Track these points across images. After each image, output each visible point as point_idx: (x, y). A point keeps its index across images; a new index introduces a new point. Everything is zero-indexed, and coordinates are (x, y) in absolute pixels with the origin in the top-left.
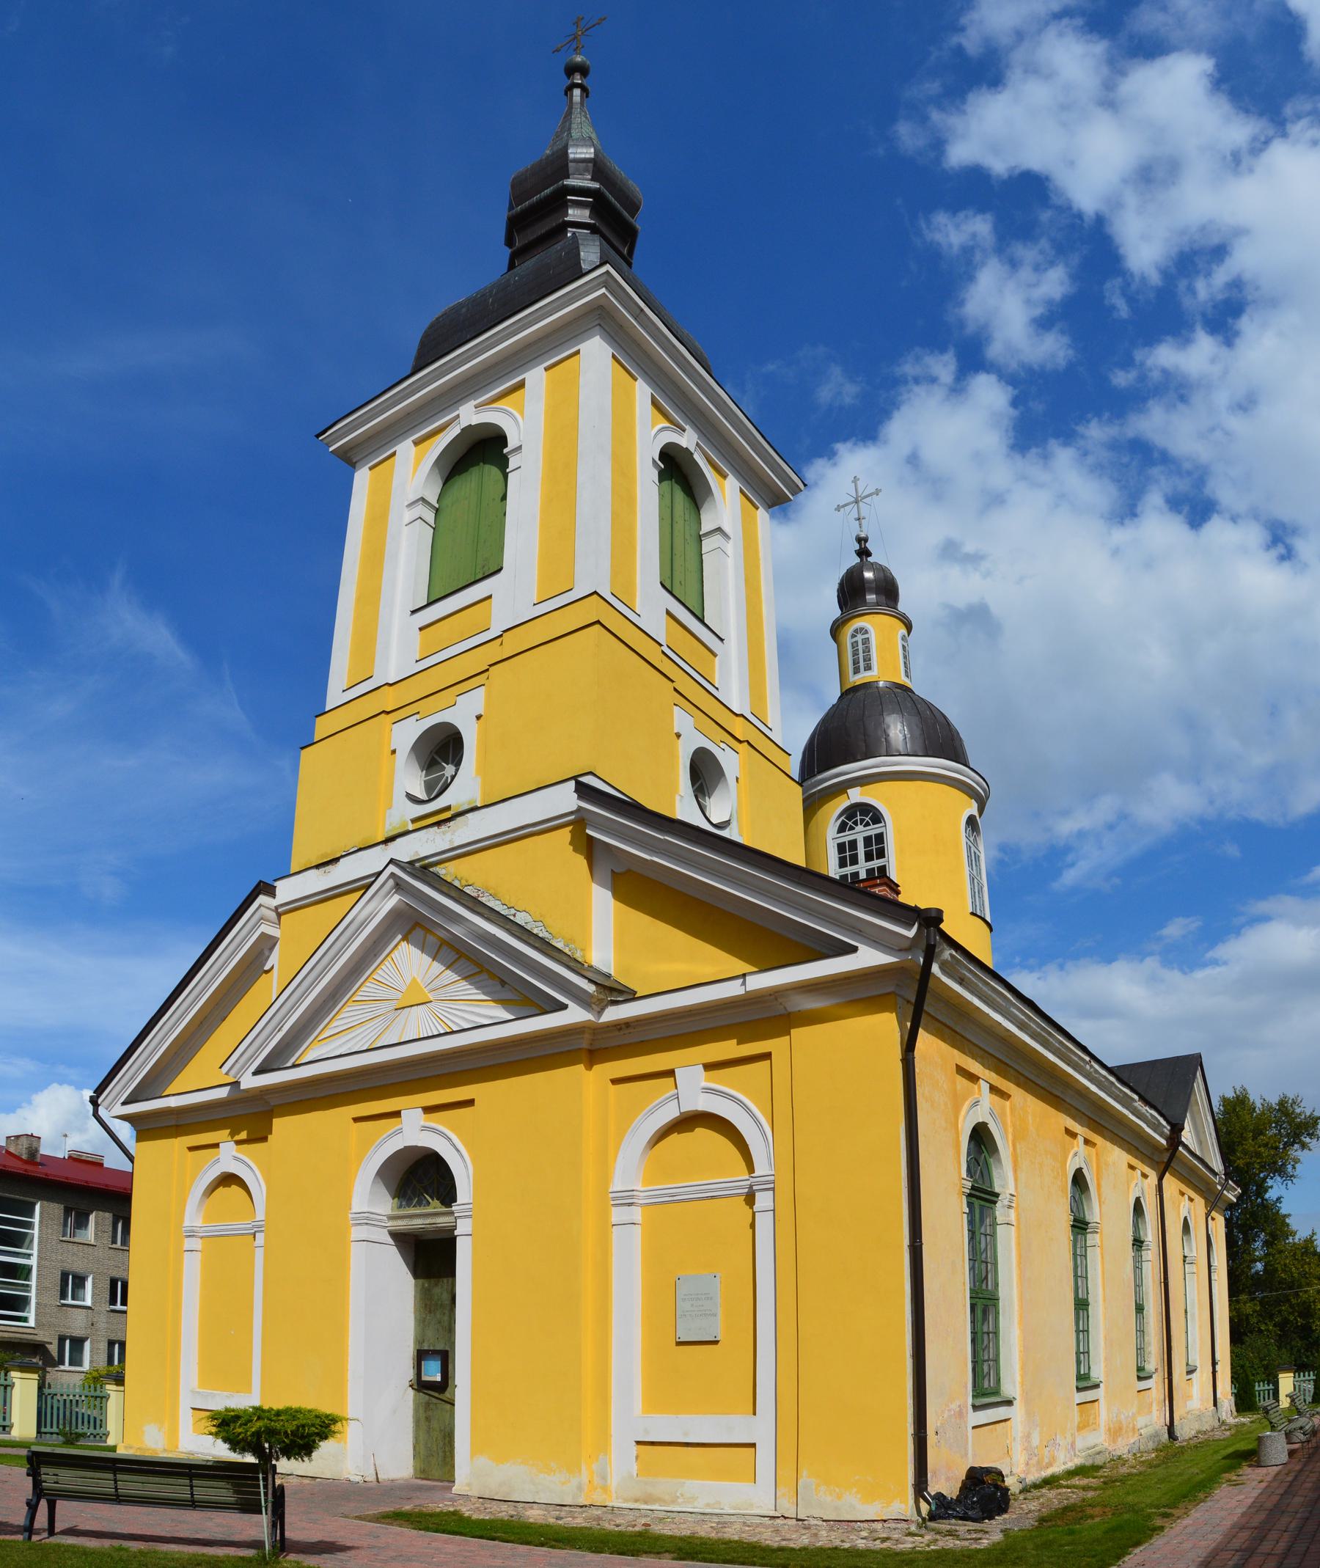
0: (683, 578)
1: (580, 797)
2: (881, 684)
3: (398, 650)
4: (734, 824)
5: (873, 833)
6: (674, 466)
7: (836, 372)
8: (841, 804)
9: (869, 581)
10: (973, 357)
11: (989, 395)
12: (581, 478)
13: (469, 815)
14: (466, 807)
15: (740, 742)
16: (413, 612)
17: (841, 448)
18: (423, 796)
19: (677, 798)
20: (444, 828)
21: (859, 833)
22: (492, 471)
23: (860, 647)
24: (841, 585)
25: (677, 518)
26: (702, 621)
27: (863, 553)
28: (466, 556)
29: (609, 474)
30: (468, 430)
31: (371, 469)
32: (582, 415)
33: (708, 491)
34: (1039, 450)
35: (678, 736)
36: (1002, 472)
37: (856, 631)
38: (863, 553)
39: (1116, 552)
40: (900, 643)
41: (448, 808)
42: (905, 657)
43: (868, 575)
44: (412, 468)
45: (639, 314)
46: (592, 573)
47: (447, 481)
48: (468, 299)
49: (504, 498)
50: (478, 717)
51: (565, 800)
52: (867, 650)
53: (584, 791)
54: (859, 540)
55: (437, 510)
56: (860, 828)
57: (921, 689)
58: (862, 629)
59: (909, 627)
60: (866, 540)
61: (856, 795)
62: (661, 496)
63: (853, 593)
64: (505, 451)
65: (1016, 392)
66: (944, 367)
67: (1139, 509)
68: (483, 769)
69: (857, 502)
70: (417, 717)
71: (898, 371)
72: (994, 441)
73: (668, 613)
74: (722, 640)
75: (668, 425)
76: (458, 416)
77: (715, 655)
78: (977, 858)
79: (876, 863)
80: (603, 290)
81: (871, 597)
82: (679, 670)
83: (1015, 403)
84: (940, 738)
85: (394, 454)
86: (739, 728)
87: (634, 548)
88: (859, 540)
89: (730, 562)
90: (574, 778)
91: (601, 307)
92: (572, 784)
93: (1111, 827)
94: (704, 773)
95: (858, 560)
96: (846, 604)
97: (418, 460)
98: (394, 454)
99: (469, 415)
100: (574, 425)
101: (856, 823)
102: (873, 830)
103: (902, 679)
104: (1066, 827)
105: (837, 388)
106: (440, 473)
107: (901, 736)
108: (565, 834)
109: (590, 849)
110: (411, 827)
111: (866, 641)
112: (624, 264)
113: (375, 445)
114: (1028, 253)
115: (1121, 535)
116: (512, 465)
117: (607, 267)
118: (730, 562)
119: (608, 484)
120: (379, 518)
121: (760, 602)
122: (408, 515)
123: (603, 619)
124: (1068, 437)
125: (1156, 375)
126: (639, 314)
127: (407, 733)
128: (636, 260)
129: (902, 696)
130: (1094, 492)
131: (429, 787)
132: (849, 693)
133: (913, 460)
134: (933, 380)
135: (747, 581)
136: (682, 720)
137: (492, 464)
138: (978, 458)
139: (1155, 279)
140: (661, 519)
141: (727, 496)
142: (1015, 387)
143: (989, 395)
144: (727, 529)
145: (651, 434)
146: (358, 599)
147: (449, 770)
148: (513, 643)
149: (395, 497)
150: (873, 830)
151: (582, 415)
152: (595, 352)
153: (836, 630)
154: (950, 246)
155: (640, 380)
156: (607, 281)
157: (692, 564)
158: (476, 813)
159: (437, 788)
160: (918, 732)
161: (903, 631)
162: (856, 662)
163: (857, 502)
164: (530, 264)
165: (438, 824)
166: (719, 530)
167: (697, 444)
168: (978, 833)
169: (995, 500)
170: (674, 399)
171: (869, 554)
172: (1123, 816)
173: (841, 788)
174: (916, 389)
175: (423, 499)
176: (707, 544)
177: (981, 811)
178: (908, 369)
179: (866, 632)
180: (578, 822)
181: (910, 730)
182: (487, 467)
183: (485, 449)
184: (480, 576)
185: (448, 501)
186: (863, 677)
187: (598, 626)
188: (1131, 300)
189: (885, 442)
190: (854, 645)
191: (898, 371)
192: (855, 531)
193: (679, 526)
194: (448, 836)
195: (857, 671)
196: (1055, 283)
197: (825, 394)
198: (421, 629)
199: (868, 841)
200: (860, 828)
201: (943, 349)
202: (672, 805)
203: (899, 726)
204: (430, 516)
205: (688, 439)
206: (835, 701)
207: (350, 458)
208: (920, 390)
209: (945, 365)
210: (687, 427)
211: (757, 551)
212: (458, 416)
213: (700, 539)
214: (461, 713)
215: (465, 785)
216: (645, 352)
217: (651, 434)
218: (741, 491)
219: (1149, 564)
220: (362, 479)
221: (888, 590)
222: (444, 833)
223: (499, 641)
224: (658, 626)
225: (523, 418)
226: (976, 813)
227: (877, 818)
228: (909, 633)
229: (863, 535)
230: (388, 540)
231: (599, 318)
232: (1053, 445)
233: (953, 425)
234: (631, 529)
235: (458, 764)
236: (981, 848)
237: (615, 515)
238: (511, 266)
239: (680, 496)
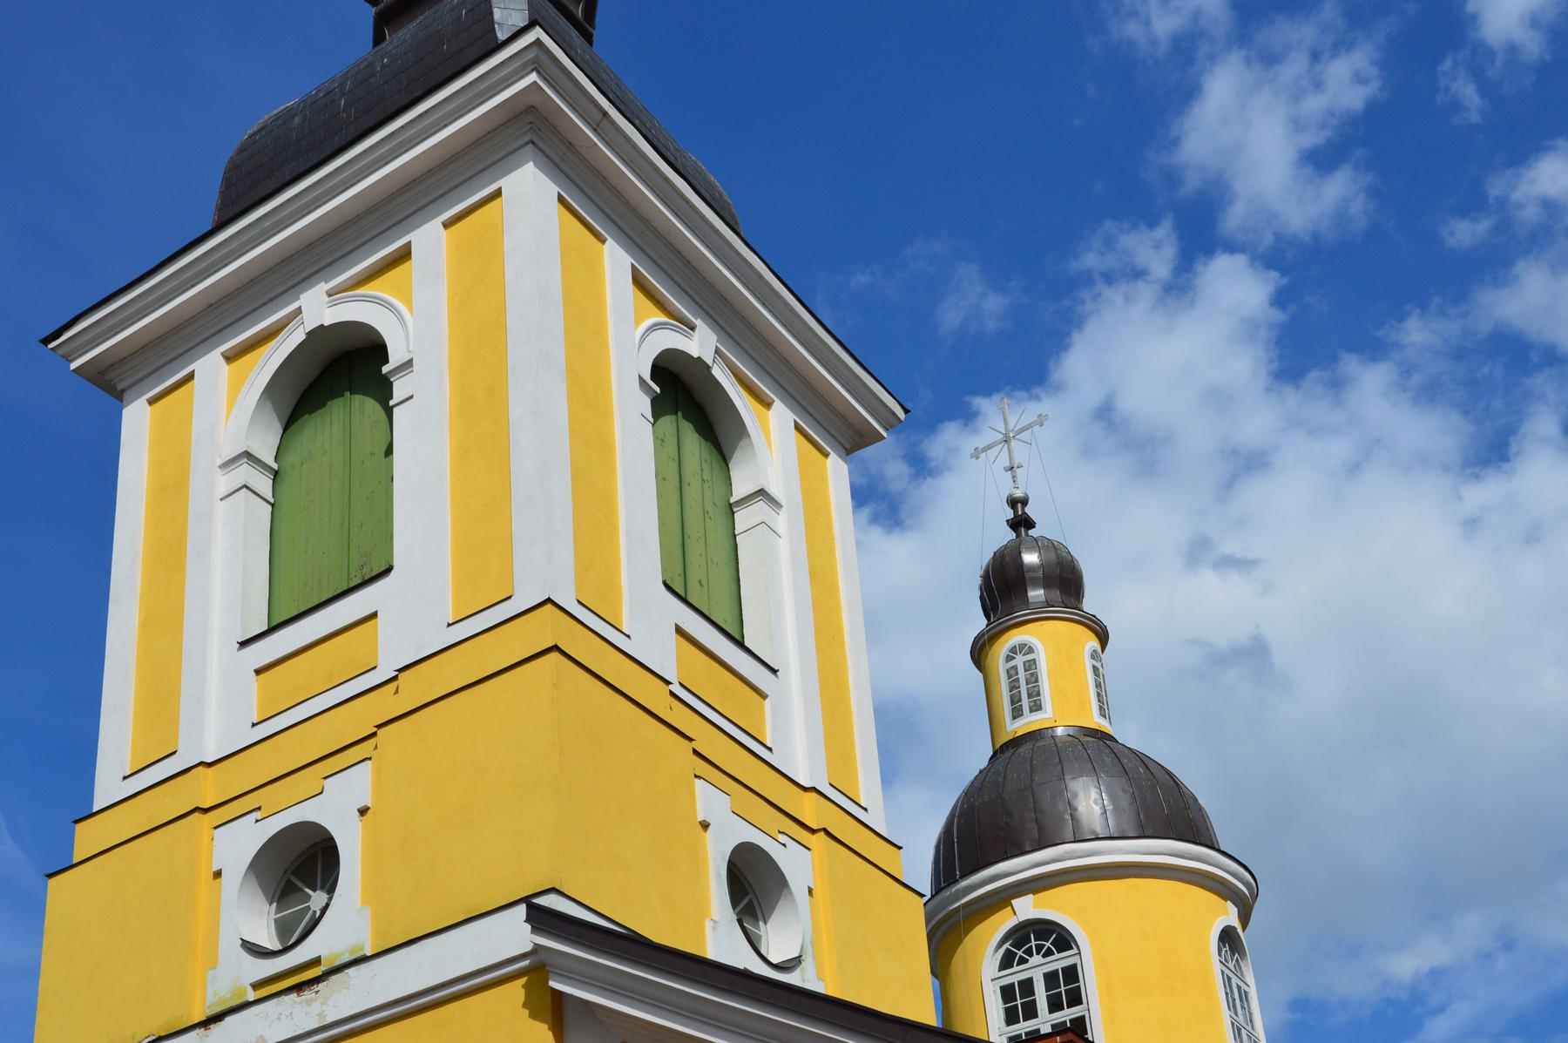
0: (703, 574)
1: (536, 929)
2: (1060, 731)
3: (220, 707)
4: (808, 962)
5: (1059, 966)
6: (679, 390)
7: (969, 273)
8: (1002, 923)
9: (1032, 568)
10: (1201, 230)
11: (1237, 288)
12: (516, 413)
13: (351, 971)
14: (347, 958)
15: (813, 831)
16: (244, 644)
17: (981, 403)
18: (273, 944)
19: (708, 925)
20: (308, 994)
21: (1036, 968)
22: (365, 406)
23: (1022, 675)
24: (986, 578)
25: (687, 478)
26: (740, 644)
27: (1021, 523)
28: (328, 554)
29: (563, 404)
30: (318, 335)
31: (151, 402)
32: (515, 306)
33: (741, 430)
34: (1326, 374)
35: (705, 826)
36: (1259, 420)
37: (1013, 650)
38: (1021, 523)
39: (1472, 524)
40: (1088, 663)
41: (316, 962)
42: (1098, 685)
43: (1030, 558)
44: (224, 400)
45: (600, 121)
46: (543, 567)
47: (290, 423)
48: (303, 101)
49: (389, 451)
50: (363, 811)
51: (512, 935)
52: (1033, 679)
53: (541, 919)
54: (1013, 502)
55: (276, 474)
56: (1036, 959)
57: (1129, 735)
58: (1022, 646)
59: (1103, 636)
60: (1025, 502)
61: (1027, 908)
62: (659, 441)
63: (1004, 590)
64: (385, 369)
65: (1285, 281)
66: (1155, 250)
67: (1514, 449)
68: (373, 893)
69: (1006, 441)
70: (258, 815)
71: (1074, 266)
72: (1244, 367)
73: (679, 631)
74: (774, 671)
75: (663, 318)
76: (299, 311)
77: (763, 696)
78: (1244, 996)
79: (1067, 1014)
80: (533, 77)
81: (1036, 594)
82: (707, 724)
83: (1280, 299)
84: (1165, 808)
85: (191, 377)
86: (809, 810)
87: (612, 526)
88: (1013, 502)
89: (783, 545)
90: (526, 900)
91: (532, 109)
92: (522, 910)
93: (1486, 957)
94: (752, 884)
95: (1012, 535)
96: (995, 609)
97: (236, 387)
98: (191, 377)
99: (318, 307)
100: (499, 322)
101: (1029, 952)
102: (1059, 962)
103: (1096, 721)
104: (1405, 966)
105: (974, 303)
106: (276, 409)
107: (1097, 809)
108: (515, 991)
109: (557, 1011)
110: (251, 996)
111: (1031, 666)
112: (574, 33)
113: (158, 359)
114: (1300, 32)
115: (1484, 493)
116: (400, 389)
117: (537, 33)
118: (783, 545)
119: (563, 420)
120: (172, 487)
121: (832, 539)
122: (224, 482)
123: (567, 643)
124: (1375, 350)
125: (1531, 213)
126: (600, 121)
127: (243, 841)
128: (597, 34)
129: (1096, 748)
130: (1430, 431)
131: (283, 928)
132: (1005, 750)
133: (1105, 413)
134: (1138, 274)
135: (813, 574)
136: (710, 800)
137: (365, 393)
138: (1219, 399)
139: (1533, 46)
140: (660, 477)
141: (772, 438)
142: (1283, 271)
143: (1237, 288)
144: (775, 490)
145: (635, 336)
146: (145, 625)
147: (317, 899)
148: (414, 690)
149: (195, 455)
150: (1059, 962)
151: (515, 306)
152: (528, 189)
153: (979, 652)
154: (1154, 43)
155: (610, 241)
156: (538, 60)
157: (720, 553)
158: (363, 967)
159: (295, 931)
160: (1125, 801)
161: (1094, 643)
162: (1016, 700)
163: (1006, 441)
164: (405, 34)
165: (298, 988)
166: (761, 493)
167: (717, 351)
168: (1243, 954)
169: (1249, 463)
170: (670, 272)
171: (1029, 524)
172: (1507, 941)
173: (1002, 899)
174: (1107, 292)
175: (247, 455)
176: (743, 518)
177: (1245, 918)
178: (1091, 260)
179: (1031, 650)
180: (536, 968)
181: (1113, 799)
182: (357, 398)
183: (347, 369)
184: (357, 581)
185: (292, 458)
186: (1029, 722)
187: (554, 655)
188: (1487, 89)
189: (1058, 389)
190: (1012, 673)
191: (1074, 266)
192: (1007, 488)
193: (693, 491)
194: (316, 1007)
195: (1017, 713)
196: (1348, 82)
197: (950, 317)
198: (258, 672)
199: (1051, 979)
200: (1036, 959)
201: (1153, 223)
202: (700, 936)
203: (1094, 794)
204: (264, 484)
205: (700, 343)
206: (984, 763)
207: (113, 382)
208: (1114, 295)
209: (1157, 247)
210: (698, 322)
211: (828, 526)
212: (299, 311)
213: (731, 510)
214: (334, 807)
215: (345, 922)
216: (616, 192)
217: (635, 336)
218: (798, 427)
219: (1532, 536)
220: (138, 420)
221: (1066, 582)
222: (309, 1003)
223: (393, 685)
224: (664, 655)
225: (410, 309)
226: (1235, 922)
227: (1064, 941)
228: (1104, 646)
229: (1019, 494)
230: (191, 522)
231: (528, 130)
232: (1350, 364)
233: (1173, 346)
234: (607, 497)
235: (331, 891)
236: (1250, 978)
237: (578, 476)
238: (378, 38)
239: (692, 441)
